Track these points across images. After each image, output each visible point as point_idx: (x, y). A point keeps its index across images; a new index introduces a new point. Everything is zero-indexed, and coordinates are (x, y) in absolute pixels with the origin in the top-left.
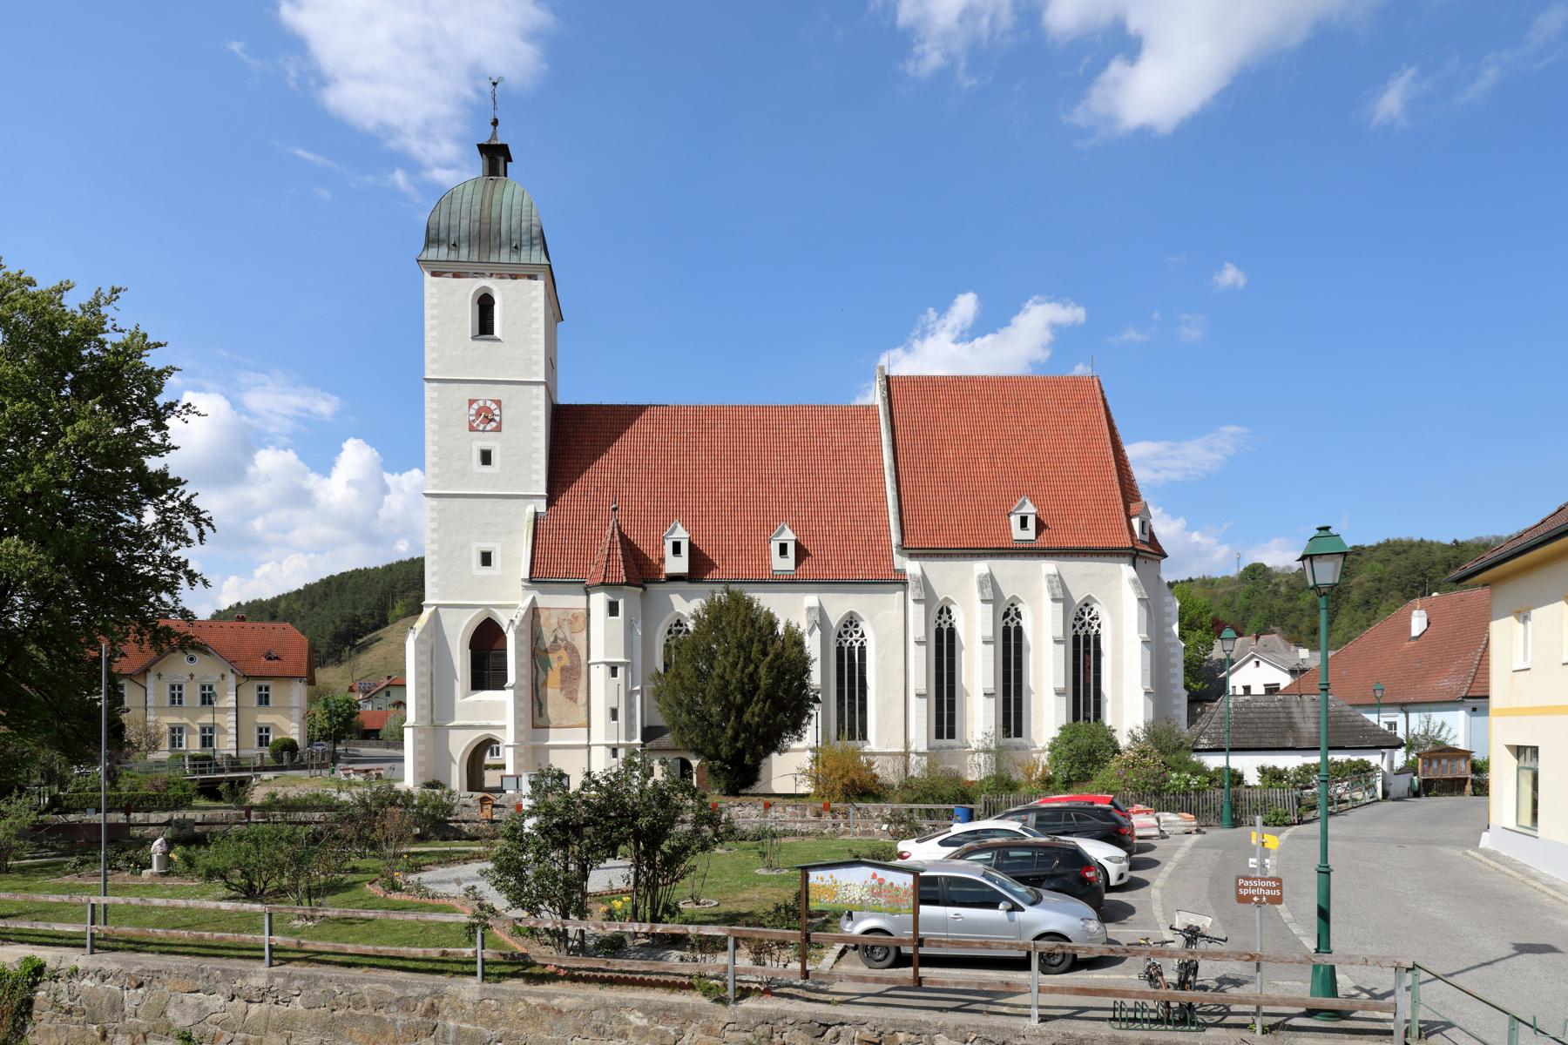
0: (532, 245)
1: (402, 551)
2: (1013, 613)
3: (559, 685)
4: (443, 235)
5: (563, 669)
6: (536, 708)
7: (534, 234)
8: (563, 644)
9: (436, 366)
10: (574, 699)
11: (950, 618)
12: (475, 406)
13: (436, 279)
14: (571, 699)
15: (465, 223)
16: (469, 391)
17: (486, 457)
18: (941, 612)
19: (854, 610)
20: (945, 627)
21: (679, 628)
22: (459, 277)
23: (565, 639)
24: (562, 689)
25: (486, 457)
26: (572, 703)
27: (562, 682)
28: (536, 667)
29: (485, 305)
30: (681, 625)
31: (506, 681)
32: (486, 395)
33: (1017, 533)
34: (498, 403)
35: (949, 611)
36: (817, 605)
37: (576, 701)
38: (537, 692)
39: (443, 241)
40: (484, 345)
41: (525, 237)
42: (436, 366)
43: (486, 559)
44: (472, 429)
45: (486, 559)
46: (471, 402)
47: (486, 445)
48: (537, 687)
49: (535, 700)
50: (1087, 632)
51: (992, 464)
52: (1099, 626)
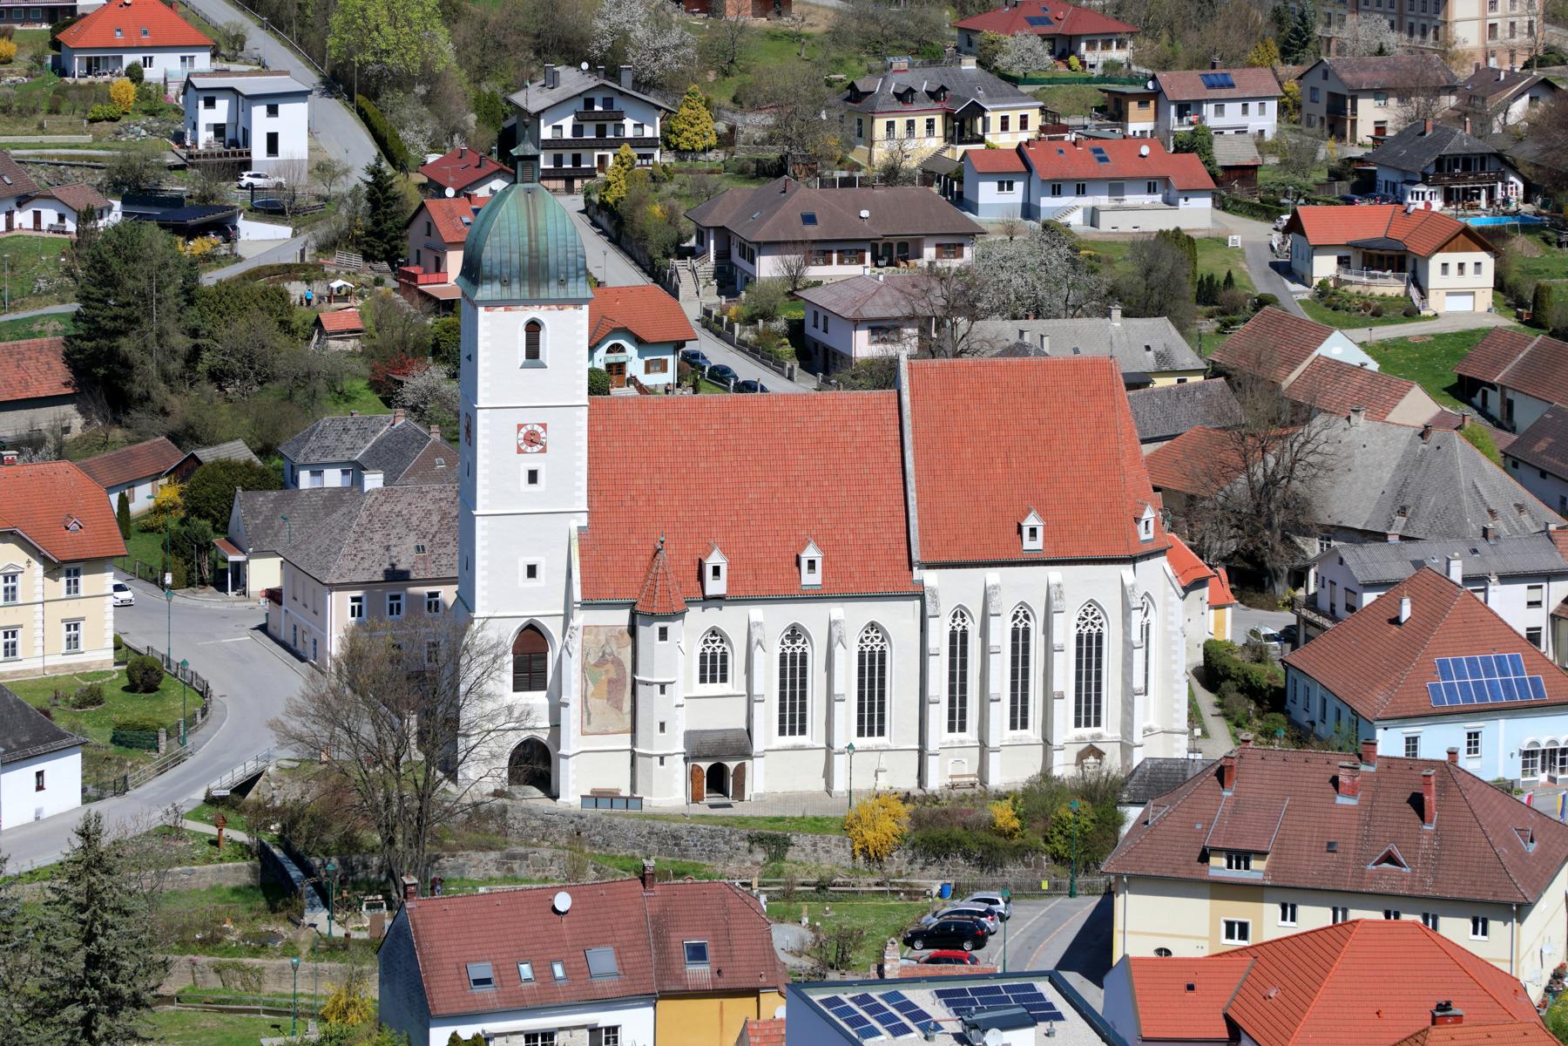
0: (577, 277)
2: (1021, 615)
3: (605, 696)
4: (496, 272)
5: (610, 681)
6: (585, 718)
7: (580, 266)
10: (619, 708)
15: (516, 257)
17: (533, 477)
18: (955, 616)
20: (959, 629)
23: (612, 654)
24: (608, 700)
25: (533, 477)
27: (609, 692)
29: (533, 328)
32: (532, 419)
33: (1028, 544)
34: (544, 426)
35: (962, 615)
37: (621, 710)
39: (496, 277)
41: (571, 269)
44: (520, 451)
46: (520, 427)
52: (1101, 625)
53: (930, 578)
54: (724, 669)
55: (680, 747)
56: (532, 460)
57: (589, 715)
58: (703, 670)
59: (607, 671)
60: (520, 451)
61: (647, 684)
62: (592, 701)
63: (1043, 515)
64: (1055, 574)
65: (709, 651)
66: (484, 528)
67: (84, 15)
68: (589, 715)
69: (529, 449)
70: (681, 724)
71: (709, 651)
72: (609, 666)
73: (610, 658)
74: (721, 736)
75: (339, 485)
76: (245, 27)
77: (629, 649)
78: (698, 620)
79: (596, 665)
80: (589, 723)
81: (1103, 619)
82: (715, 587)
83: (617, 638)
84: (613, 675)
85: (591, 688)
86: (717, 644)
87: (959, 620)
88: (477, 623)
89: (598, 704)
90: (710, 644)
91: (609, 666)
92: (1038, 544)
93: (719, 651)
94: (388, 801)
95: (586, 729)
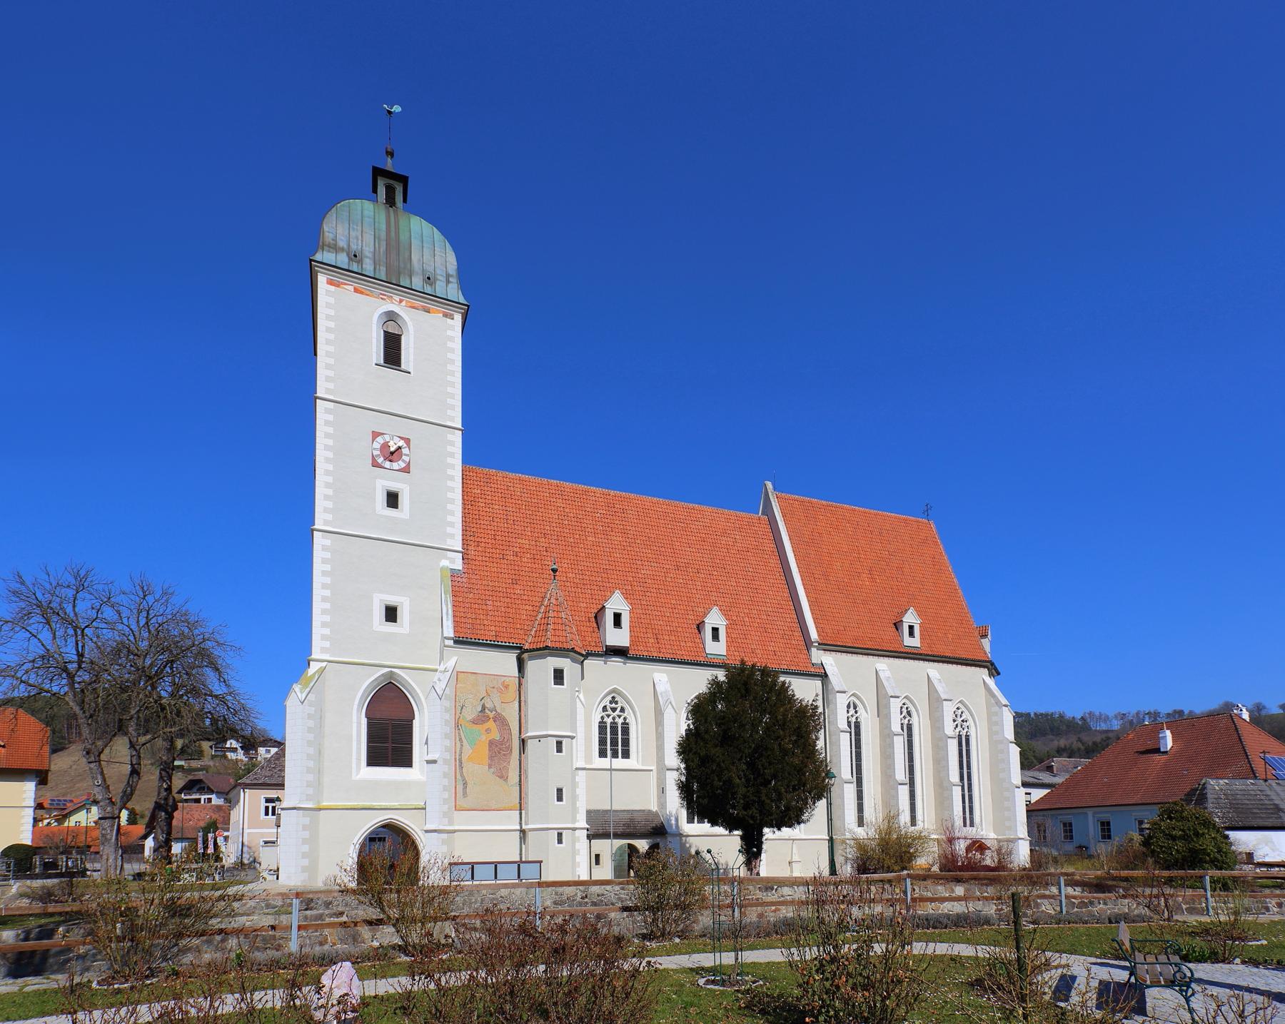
1: (398, 620)
3: (486, 761)
5: (491, 743)
6: (460, 787)
8: (492, 715)
9: (331, 386)
10: (503, 777)
11: (856, 712)
12: (380, 440)
13: (332, 288)
14: (501, 777)
16: (381, 423)
17: (393, 500)
18: (849, 706)
19: (1257, 701)
20: (853, 720)
21: (613, 705)
22: (362, 293)
24: (490, 766)
25: (393, 500)
26: (501, 781)
27: (491, 758)
28: (460, 739)
30: (616, 703)
31: (700, 709)
33: (908, 641)
34: (407, 441)
35: (855, 707)
36: (325, 252)
37: (506, 780)
38: (461, 768)
40: (390, 373)
42: (331, 386)
43: (391, 614)
45: (391, 614)
46: (376, 435)
47: (394, 486)
48: (461, 762)
49: (459, 776)
50: (960, 732)
51: (873, 579)
53: (829, 661)
54: (626, 743)
55: (583, 823)
56: (387, 480)
57: (465, 784)
58: (602, 742)
59: (488, 731)
60: (376, 435)
61: (539, 737)
62: (469, 768)
63: (725, 613)
64: (934, 671)
65: (609, 721)
66: (324, 548)
67: (1015, 712)
68: (465, 784)
69: (387, 464)
70: (584, 799)
71: (609, 721)
72: (491, 724)
73: (492, 715)
74: (627, 816)
75: (29, 843)
76: (777, 832)
77: (448, 552)
78: (605, 674)
79: (475, 722)
80: (465, 794)
81: (970, 722)
82: (617, 637)
83: (501, 692)
84: (496, 735)
85: (468, 750)
86: (617, 712)
87: (852, 711)
88: (314, 667)
89: (478, 770)
90: (610, 712)
91: (491, 724)
92: (915, 642)
93: (620, 721)
94: (200, 908)
95: (461, 802)
